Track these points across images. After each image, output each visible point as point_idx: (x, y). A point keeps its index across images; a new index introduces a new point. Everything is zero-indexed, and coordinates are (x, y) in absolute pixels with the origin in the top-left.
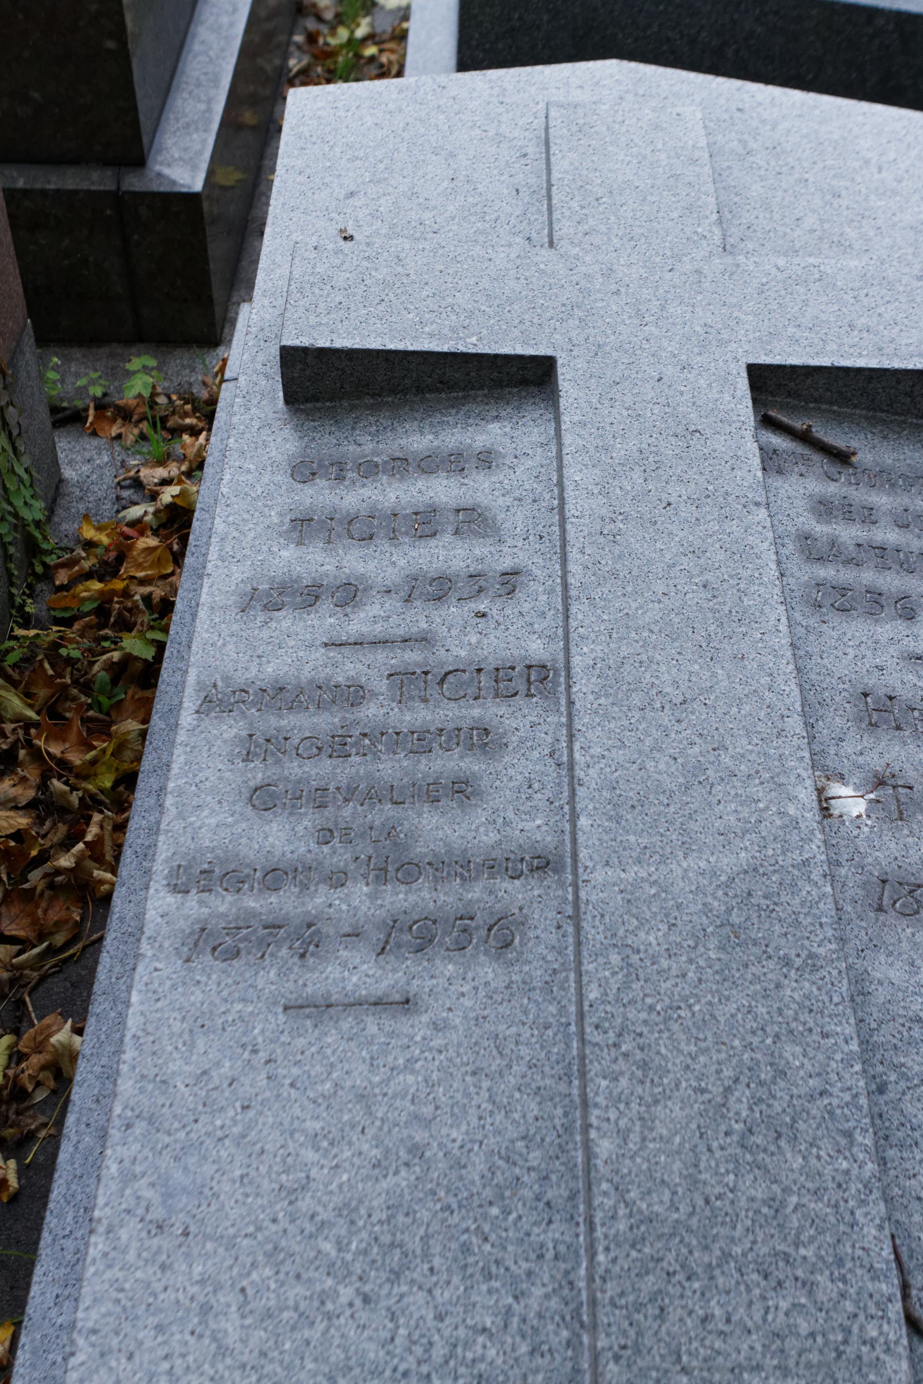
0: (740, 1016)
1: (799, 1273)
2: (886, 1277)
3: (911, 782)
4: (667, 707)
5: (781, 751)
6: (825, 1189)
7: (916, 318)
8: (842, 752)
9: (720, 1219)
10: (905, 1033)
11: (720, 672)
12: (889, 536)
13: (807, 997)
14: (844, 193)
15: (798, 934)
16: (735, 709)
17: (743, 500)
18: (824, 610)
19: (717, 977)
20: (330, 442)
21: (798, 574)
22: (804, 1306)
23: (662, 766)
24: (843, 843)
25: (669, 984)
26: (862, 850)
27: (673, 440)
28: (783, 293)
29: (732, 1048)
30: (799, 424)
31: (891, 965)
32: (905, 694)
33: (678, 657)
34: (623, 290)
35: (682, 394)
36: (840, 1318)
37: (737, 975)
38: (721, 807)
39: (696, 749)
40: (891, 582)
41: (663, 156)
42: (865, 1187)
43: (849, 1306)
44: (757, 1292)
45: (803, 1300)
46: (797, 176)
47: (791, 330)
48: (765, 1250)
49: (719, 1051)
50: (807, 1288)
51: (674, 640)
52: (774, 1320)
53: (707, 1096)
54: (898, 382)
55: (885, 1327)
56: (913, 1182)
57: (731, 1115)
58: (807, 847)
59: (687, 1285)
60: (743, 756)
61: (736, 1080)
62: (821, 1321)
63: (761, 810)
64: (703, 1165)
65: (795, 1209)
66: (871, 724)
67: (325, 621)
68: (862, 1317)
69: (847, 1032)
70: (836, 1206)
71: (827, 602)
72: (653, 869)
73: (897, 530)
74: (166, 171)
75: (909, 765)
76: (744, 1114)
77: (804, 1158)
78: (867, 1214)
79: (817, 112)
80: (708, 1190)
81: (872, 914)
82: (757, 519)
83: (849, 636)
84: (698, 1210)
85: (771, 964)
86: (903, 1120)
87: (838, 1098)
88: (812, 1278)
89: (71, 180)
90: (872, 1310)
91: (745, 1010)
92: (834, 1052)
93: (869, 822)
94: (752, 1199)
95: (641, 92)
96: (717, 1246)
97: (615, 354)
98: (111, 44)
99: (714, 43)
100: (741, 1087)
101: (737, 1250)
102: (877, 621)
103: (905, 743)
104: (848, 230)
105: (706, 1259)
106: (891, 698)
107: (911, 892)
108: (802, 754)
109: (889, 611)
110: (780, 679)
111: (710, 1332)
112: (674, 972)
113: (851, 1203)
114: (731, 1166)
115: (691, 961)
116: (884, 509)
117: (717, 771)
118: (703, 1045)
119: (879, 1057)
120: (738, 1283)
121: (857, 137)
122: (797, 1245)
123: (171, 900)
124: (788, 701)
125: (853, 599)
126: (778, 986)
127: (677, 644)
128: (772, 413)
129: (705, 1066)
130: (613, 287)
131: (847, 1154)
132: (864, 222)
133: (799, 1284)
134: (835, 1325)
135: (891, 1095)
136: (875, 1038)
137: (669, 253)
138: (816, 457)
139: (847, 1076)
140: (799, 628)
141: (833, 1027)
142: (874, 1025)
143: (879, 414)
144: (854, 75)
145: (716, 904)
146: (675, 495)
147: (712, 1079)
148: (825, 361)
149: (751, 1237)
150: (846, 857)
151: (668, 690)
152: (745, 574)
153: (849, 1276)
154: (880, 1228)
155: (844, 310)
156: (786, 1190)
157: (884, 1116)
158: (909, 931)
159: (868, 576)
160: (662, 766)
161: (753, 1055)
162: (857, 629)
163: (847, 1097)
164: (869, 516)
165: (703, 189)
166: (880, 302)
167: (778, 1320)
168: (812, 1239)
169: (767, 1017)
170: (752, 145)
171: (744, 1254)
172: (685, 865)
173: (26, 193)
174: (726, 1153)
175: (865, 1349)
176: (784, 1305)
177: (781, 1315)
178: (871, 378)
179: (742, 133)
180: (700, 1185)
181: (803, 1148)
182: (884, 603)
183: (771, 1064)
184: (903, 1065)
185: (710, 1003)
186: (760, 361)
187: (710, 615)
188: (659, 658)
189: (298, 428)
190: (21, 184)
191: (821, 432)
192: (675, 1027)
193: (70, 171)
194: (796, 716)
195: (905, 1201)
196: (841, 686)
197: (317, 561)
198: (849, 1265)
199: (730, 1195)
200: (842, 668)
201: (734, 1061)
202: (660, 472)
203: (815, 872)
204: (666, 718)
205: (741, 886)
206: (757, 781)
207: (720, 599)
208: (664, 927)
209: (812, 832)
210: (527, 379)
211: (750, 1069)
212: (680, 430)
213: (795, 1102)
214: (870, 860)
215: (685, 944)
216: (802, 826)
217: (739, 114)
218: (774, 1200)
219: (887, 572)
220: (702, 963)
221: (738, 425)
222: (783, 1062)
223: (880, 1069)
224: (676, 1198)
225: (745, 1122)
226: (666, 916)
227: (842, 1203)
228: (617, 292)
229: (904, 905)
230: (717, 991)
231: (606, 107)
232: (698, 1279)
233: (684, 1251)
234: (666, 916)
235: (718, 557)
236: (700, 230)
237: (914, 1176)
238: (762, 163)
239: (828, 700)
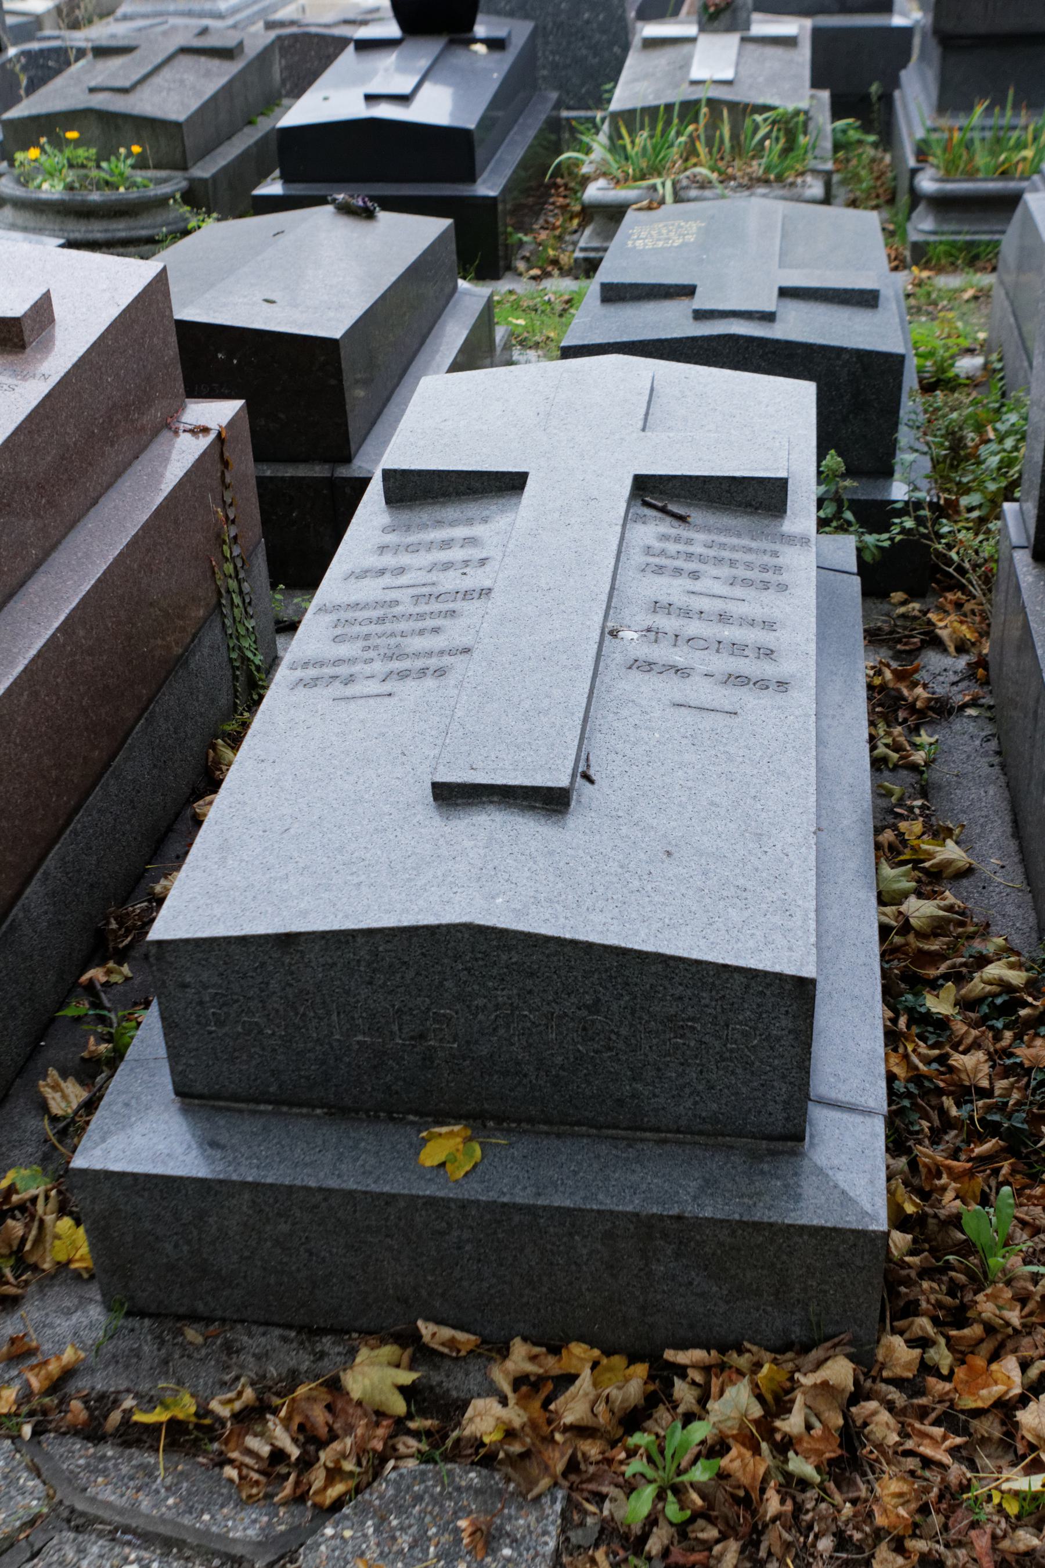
12: (697, 549)
20: (405, 516)
30: (660, 504)
67: (387, 580)
74: (364, 465)
89: (302, 471)
98: (333, 382)
123: (288, 672)
128: (647, 499)
173: (271, 479)
189: (391, 514)
190: (268, 473)
193: (302, 466)
197: (388, 560)
210: (511, 484)
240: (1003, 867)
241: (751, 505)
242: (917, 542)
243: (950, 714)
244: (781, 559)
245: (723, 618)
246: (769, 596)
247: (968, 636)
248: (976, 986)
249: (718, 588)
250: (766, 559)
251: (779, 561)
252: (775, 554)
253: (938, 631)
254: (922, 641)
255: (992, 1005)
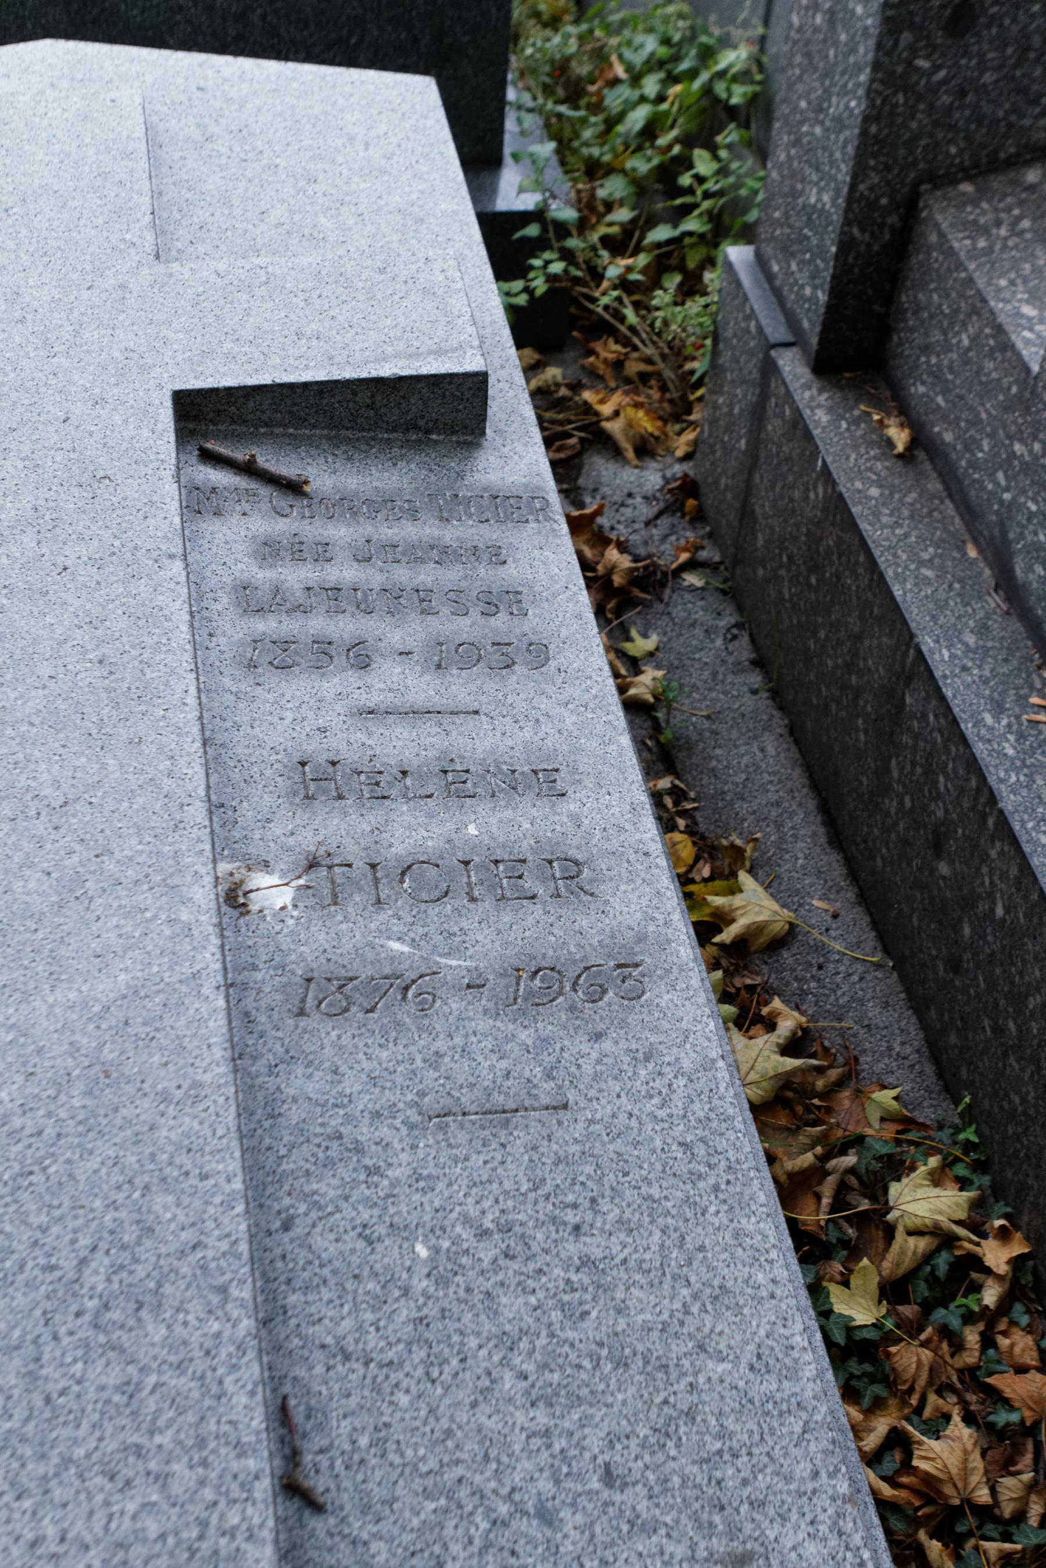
0: (104, 1171)
1: (153, 1466)
2: (255, 1451)
3: (351, 858)
4: (44, 813)
5: (177, 847)
6: (191, 1360)
7: (374, 318)
8: (269, 835)
9: (61, 1419)
10: (321, 1155)
11: (111, 762)
12: (344, 572)
13: (186, 1135)
14: (321, 177)
15: (181, 1062)
16: (126, 804)
17: (155, 554)
18: (260, 670)
19: (80, 1128)
21: (229, 633)
22: (154, 1504)
23: (32, 885)
24: (261, 942)
25: (20, 1147)
26: (284, 947)
27: (76, 491)
28: (222, 302)
29: (92, 1210)
30: (240, 455)
31: (310, 1076)
32: (350, 756)
33: (61, 751)
34: (29, 317)
35: (91, 434)
36: (196, 1510)
37: (105, 1122)
38: (100, 924)
39: (75, 858)
40: (344, 627)
41: (91, 152)
42: (238, 1348)
43: (208, 1494)
44: (99, 1498)
45: (154, 1498)
46: (265, 162)
47: (228, 345)
48: (113, 1446)
49: (76, 1217)
50: (161, 1481)
51: (58, 731)
52: (118, 1527)
53: (58, 1273)
54: (355, 394)
55: (250, 1511)
56: (317, 1328)
57: (84, 1291)
58: (199, 956)
59: (16, 1505)
60: (130, 859)
61: (94, 1249)
62: (174, 1518)
63: (148, 921)
64: (46, 1357)
65: (153, 1391)
66: (307, 797)
68: (222, 1504)
69: (230, 1168)
70: (202, 1377)
71: (265, 660)
72: (11, 1011)
73: (355, 565)
75: (349, 839)
76: (100, 1288)
77: (168, 1327)
78: (237, 1381)
79: (295, 85)
80: (50, 1386)
81: (291, 1022)
82: (169, 574)
83: (288, 697)
84: (36, 1413)
85: (146, 1103)
86: (310, 1256)
87: (216, 1245)
88: (167, 1469)
90: (236, 1492)
91: (111, 1162)
92: (214, 1195)
93: (295, 913)
94: (102, 1388)
95: (79, 76)
96: (56, 1451)
97: (14, 395)
99: (234, 9)
100: (99, 1255)
101: (79, 1452)
102: (323, 675)
103: (346, 814)
104: (322, 220)
105: (42, 1470)
106: (334, 764)
107: (341, 987)
108: (201, 846)
109: (340, 660)
110: (182, 762)
111: (40, 1558)
112: (28, 1131)
113: (220, 1371)
114: (80, 1353)
115: (49, 1115)
116: (341, 542)
117: (99, 881)
118: (57, 1213)
119: (287, 1188)
120: (78, 1492)
121: (342, 110)
122: (151, 1433)
124: (189, 786)
125: (296, 652)
126: (152, 1128)
127: (61, 736)
129: (58, 1238)
130: (18, 315)
131: (220, 1313)
132: (343, 209)
133: (151, 1479)
134: (191, 1518)
135: (298, 1230)
136: (284, 1166)
137: (89, 268)
138: (265, 491)
139: (226, 1221)
140: (228, 695)
141: (214, 1165)
142: (283, 1151)
143: (343, 432)
144: (403, 35)
145: (85, 1041)
146: (73, 557)
147: (65, 1253)
148: (265, 379)
149: (97, 1434)
150: (264, 958)
151: (46, 791)
152: (150, 641)
153: (211, 1458)
154: (253, 1393)
155: (292, 316)
156: (144, 1370)
157: (289, 1257)
158: (334, 1033)
159: (317, 624)
160: (32, 885)
161: (117, 1215)
162: (299, 687)
163: (224, 1246)
164: (323, 553)
165: (136, 187)
166: (334, 302)
167: (123, 1527)
168: (170, 1422)
169: (136, 1166)
170: (213, 129)
171: (88, 1456)
172: (51, 999)
174: (76, 1338)
175: (223, 1541)
176: (131, 1507)
177: (127, 1519)
178: (321, 392)
179: (202, 116)
180: (40, 1383)
181: (167, 1315)
182: (333, 653)
183: (138, 1222)
184: (315, 1193)
185: (69, 1161)
186: (189, 386)
187: (104, 695)
188: (37, 754)
191: (268, 460)
192: (24, 1196)
194: (198, 803)
195: (306, 1352)
196: (274, 757)
198: (212, 1445)
199: (76, 1388)
200: (274, 738)
201: (94, 1225)
202: (58, 531)
203: (207, 985)
204: (40, 827)
205: (116, 1015)
206: (146, 887)
207: (118, 676)
208: (20, 1079)
209: (207, 938)
211: (112, 1232)
212: (86, 479)
213: (162, 1262)
214: (293, 957)
215: (44, 1095)
216: (195, 932)
217: (200, 94)
218: (128, 1383)
219: (341, 616)
220: (63, 1114)
221: (156, 464)
222: (151, 1217)
223: (287, 1201)
224: (10, 1404)
225: (101, 1296)
226: (24, 1064)
227: (209, 1374)
228: (22, 321)
229: (329, 1005)
230: (79, 1145)
231: (26, 98)
232: (30, 1496)
233: (15, 1465)
234: (24, 1064)
235: (120, 625)
236: (128, 237)
237: (320, 1320)
238: (224, 150)
239: (257, 777)
240: (835, 916)
241: (416, 428)
242: (567, 291)
243: (663, 585)
244: (511, 568)
245: (455, 782)
246: (519, 686)
247: (650, 429)
248: (903, 1252)
249: (421, 687)
250: (485, 573)
251: (512, 573)
252: (497, 557)
253: (607, 425)
254: (582, 440)
255: (932, 1280)
